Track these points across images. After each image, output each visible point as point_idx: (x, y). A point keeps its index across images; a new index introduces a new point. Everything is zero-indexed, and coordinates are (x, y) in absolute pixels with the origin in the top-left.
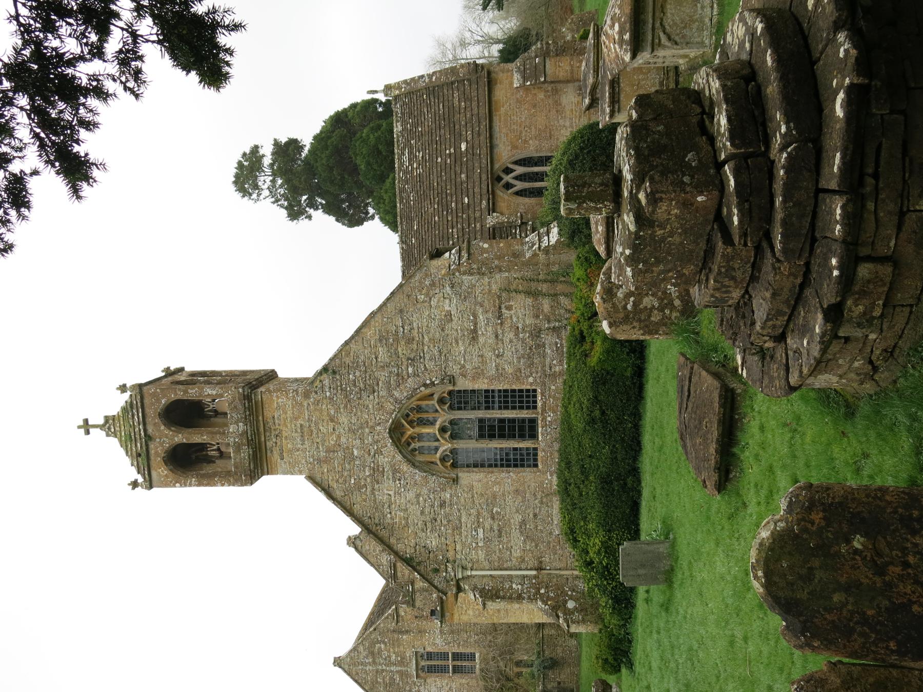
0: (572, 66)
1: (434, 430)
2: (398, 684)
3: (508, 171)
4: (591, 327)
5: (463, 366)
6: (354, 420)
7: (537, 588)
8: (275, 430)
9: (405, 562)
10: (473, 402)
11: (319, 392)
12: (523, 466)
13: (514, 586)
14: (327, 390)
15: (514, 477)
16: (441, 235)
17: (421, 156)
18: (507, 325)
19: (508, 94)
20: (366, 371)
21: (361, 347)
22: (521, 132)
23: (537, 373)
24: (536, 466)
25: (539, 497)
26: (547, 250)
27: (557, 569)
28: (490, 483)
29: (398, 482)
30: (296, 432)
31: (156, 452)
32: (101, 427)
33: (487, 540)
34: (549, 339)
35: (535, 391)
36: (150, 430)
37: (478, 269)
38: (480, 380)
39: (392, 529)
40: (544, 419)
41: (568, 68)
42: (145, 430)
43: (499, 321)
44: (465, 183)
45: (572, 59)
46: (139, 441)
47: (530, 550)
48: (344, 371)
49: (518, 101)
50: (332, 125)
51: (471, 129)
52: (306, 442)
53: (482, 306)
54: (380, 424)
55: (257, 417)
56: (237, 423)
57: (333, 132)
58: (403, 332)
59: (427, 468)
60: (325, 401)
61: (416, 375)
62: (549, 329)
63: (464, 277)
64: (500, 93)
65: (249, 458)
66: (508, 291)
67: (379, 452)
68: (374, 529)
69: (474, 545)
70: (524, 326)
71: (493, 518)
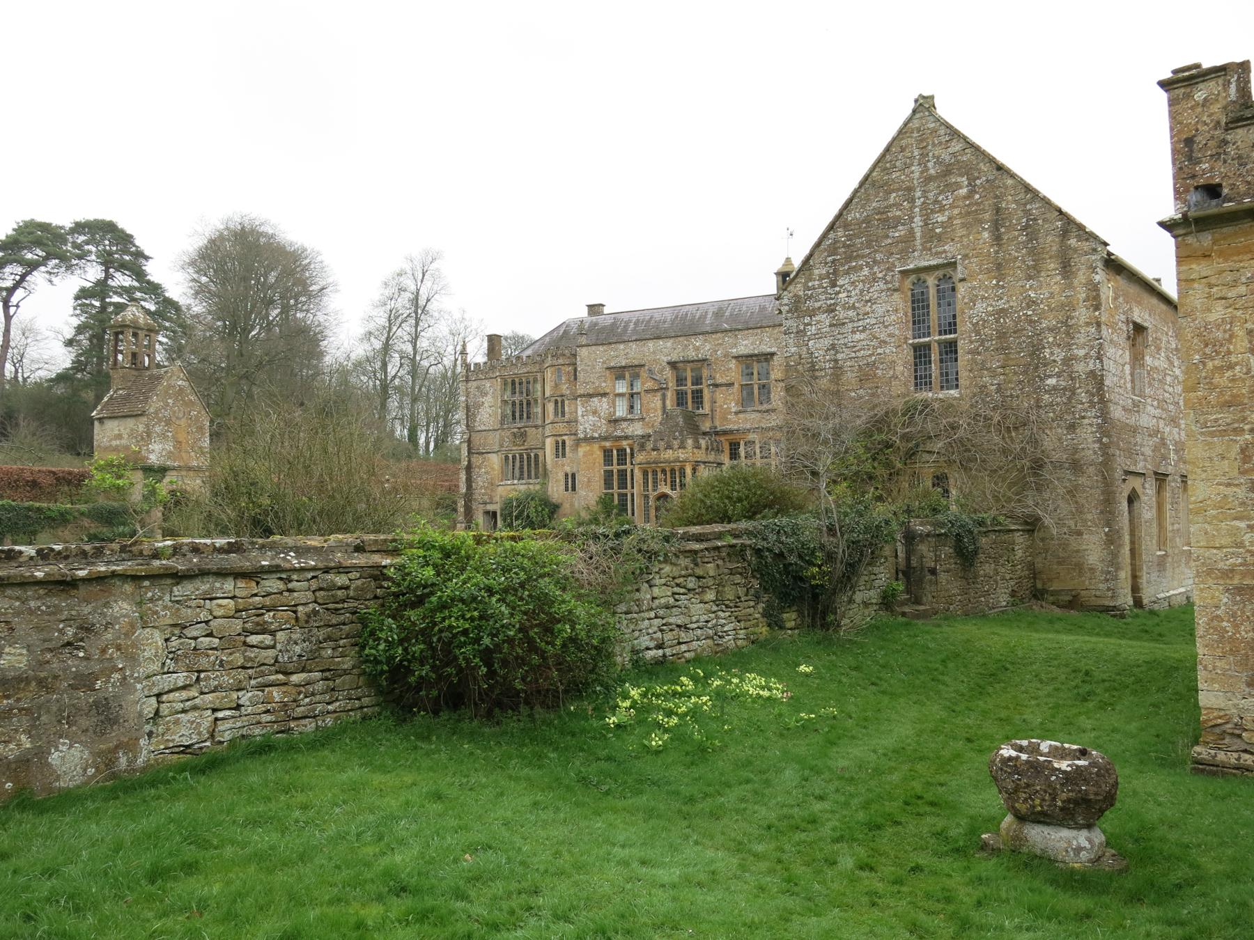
2: (887, 237)
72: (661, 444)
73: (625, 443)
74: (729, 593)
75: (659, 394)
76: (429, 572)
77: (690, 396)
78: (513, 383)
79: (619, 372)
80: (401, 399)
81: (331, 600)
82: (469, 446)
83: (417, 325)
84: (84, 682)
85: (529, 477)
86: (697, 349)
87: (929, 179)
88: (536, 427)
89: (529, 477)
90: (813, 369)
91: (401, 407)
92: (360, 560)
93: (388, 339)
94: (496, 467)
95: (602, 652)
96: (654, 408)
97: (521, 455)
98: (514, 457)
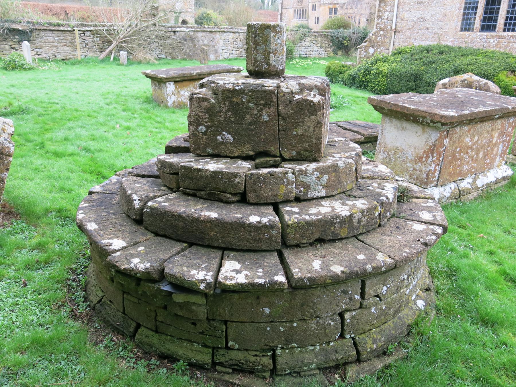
12: (463, 19)
13: (387, 13)
15: (455, 13)
24: (461, 30)
25: (439, 32)
40: (493, 37)
47: (407, 24)
72: (349, 7)
73: (337, 6)
84: (214, 46)
98: (298, 10)
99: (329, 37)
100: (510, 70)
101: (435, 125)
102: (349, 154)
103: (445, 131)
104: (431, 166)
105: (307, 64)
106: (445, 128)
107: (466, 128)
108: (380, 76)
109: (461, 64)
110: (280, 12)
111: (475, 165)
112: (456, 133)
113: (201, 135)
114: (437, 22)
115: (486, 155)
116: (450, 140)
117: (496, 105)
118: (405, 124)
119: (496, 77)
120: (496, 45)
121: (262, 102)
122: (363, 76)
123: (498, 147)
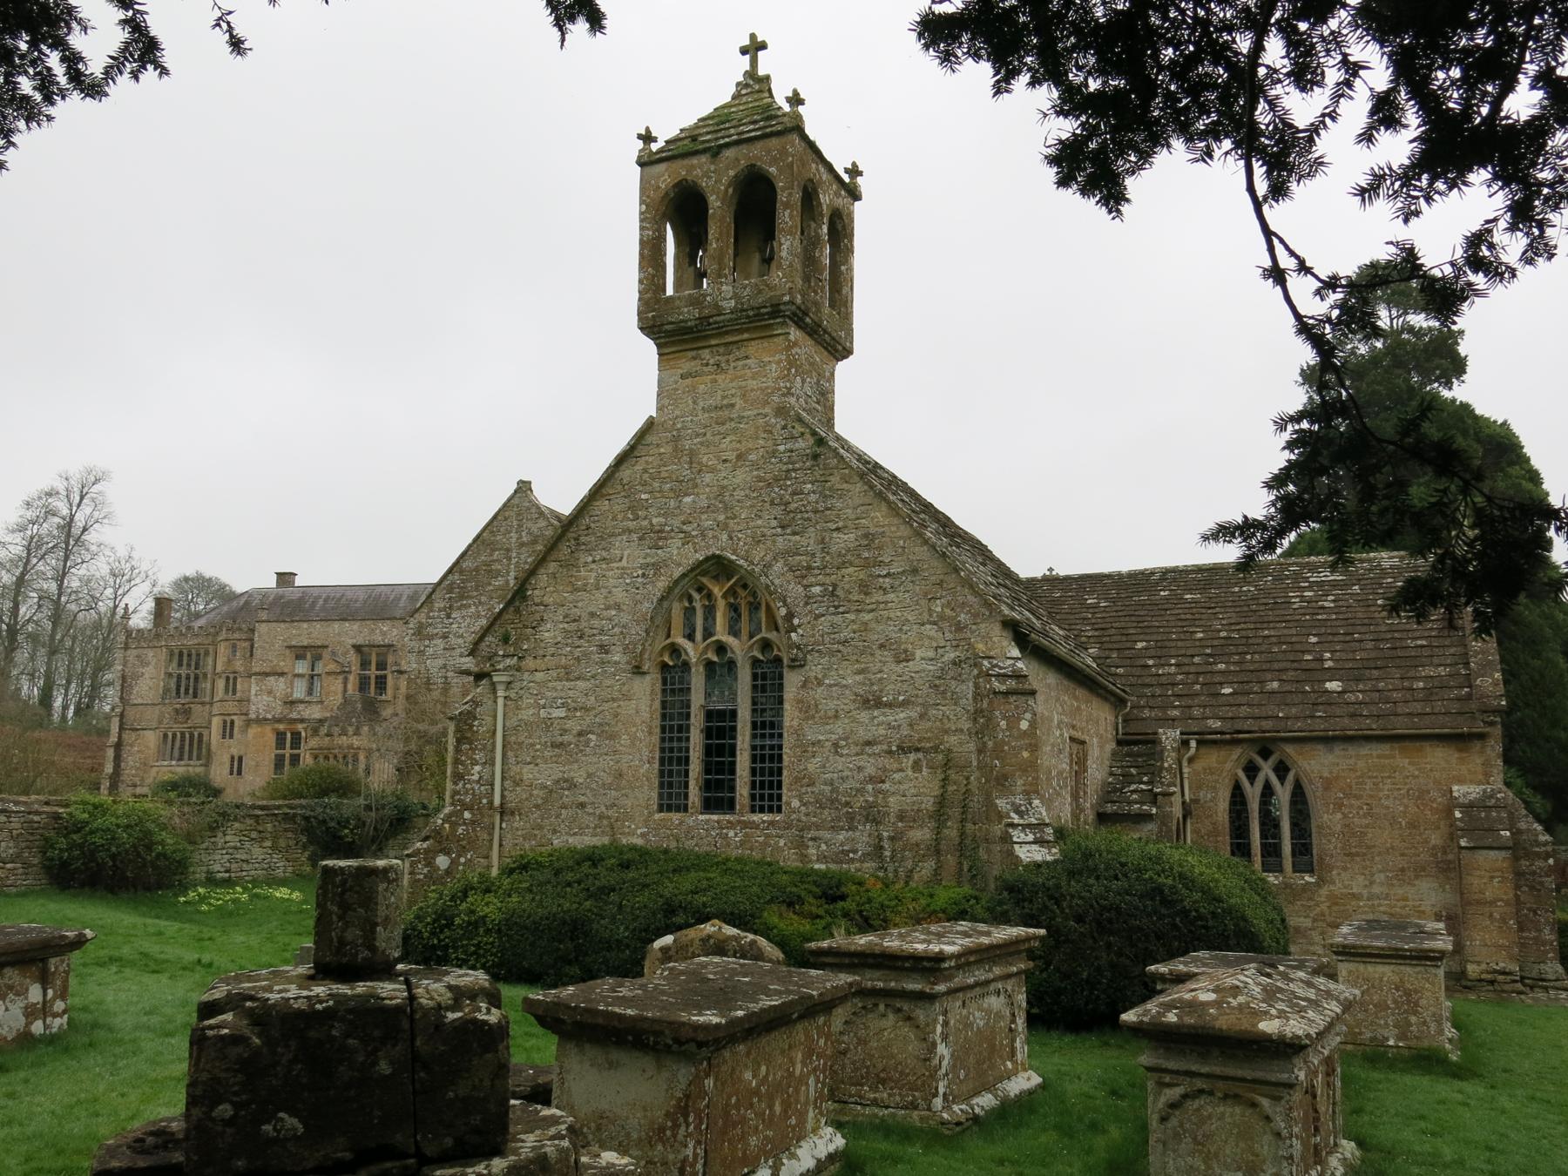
0: (1492, 903)
1: (721, 634)
2: (490, 584)
3: (1282, 770)
4: (846, 915)
5: (820, 683)
6: (739, 494)
7: (473, 805)
8: (728, 361)
9: (519, 589)
10: (764, 700)
11: (786, 433)
12: (661, 785)
13: (477, 768)
14: (788, 446)
16: (1167, 643)
17: (1326, 604)
18: (888, 762)
19: (1437, 775)
20: (816, 512)
21: (858, 501)
22: (1358, 797)
23: (807, 815)
24: (661, 810)
25: (610, 813)
26: (1006, 839)
27: (501, 840)
28: (634, 729)
29: (640, 572)
30: (724, 397)
31: (693, 167)
32: (751, 74)
33: (548, 723)
34: (862, 837)
35: (779, 810)
36: (729, 153)
37: (982, 711)
38: (797, 713)
39: (571, 564)
40: (731, 825)
41: (1488, 895)
42: (727, 145)
43: (894, 748)
44: (1262, 688)
45: (1507, 903)
46: (715, 136)
47: (531, 795)
48: (818, 473)
49: (1423, 793)
50: (1490, 437)
51: (1367, 700)
52: (706, 415)
53: (922, 716)
54: (731, 538)
55: (747, 330)
56: (735, 296)
57: (1479, 441)
58: (879, 576)
59: (659, 621)
60: (770, 443)
61: (808, 599)
62: (880, 838)
63: (971, 684)
64: (1439, 758)
65: (682, 321)
66: (947, 765)
67: (687, 538)
68: (571, 535)
69: (542, 702)
70: (885, 793)
71: (580, 734)
72: (336, 730)
73: (300, 727)
74: (282, 843)
75: (341, 677)
76: (86, 815)
77: (373, 681)
78: (181, 654)
79: (300, 652)
80: (34, 650)
81: (30, 827)
82: (121, 721)
83: (66, 558)
85: (190, 759)
86: (384, 634)
87: (522, 545)
88: (203, 704)
89: (190, 759)
90: (428, 683)
91: (32, 658)
92: (46, 809)
93: (23, 574)
94: (152, 745)
95: (182, 865)
96: (334, 692)
97: (183, 734)
98: (174, 736)
99: (298, 820)
100: (784, 901)
101: (683, 1048)
102: (552, 1131)
103: (704, 1059)
104: (686, 1146)
105: (235, 901)
106: (705, 1052)
107: (741, 1048)
108: (481, 930)
109: (677, 892)
110: (114, 739)
111: (770, 1133)
112: (725, 1062)
113: (220, 1128)
114: (602, 791)
115: (786, 1106)
116: (716, 1080)
117: (789, 992)
118: (616, 1055)
119: (760, 917)
120: (742, 843)
121: (377, 1033)
122: (433, 933)
123: (807, 1084)
